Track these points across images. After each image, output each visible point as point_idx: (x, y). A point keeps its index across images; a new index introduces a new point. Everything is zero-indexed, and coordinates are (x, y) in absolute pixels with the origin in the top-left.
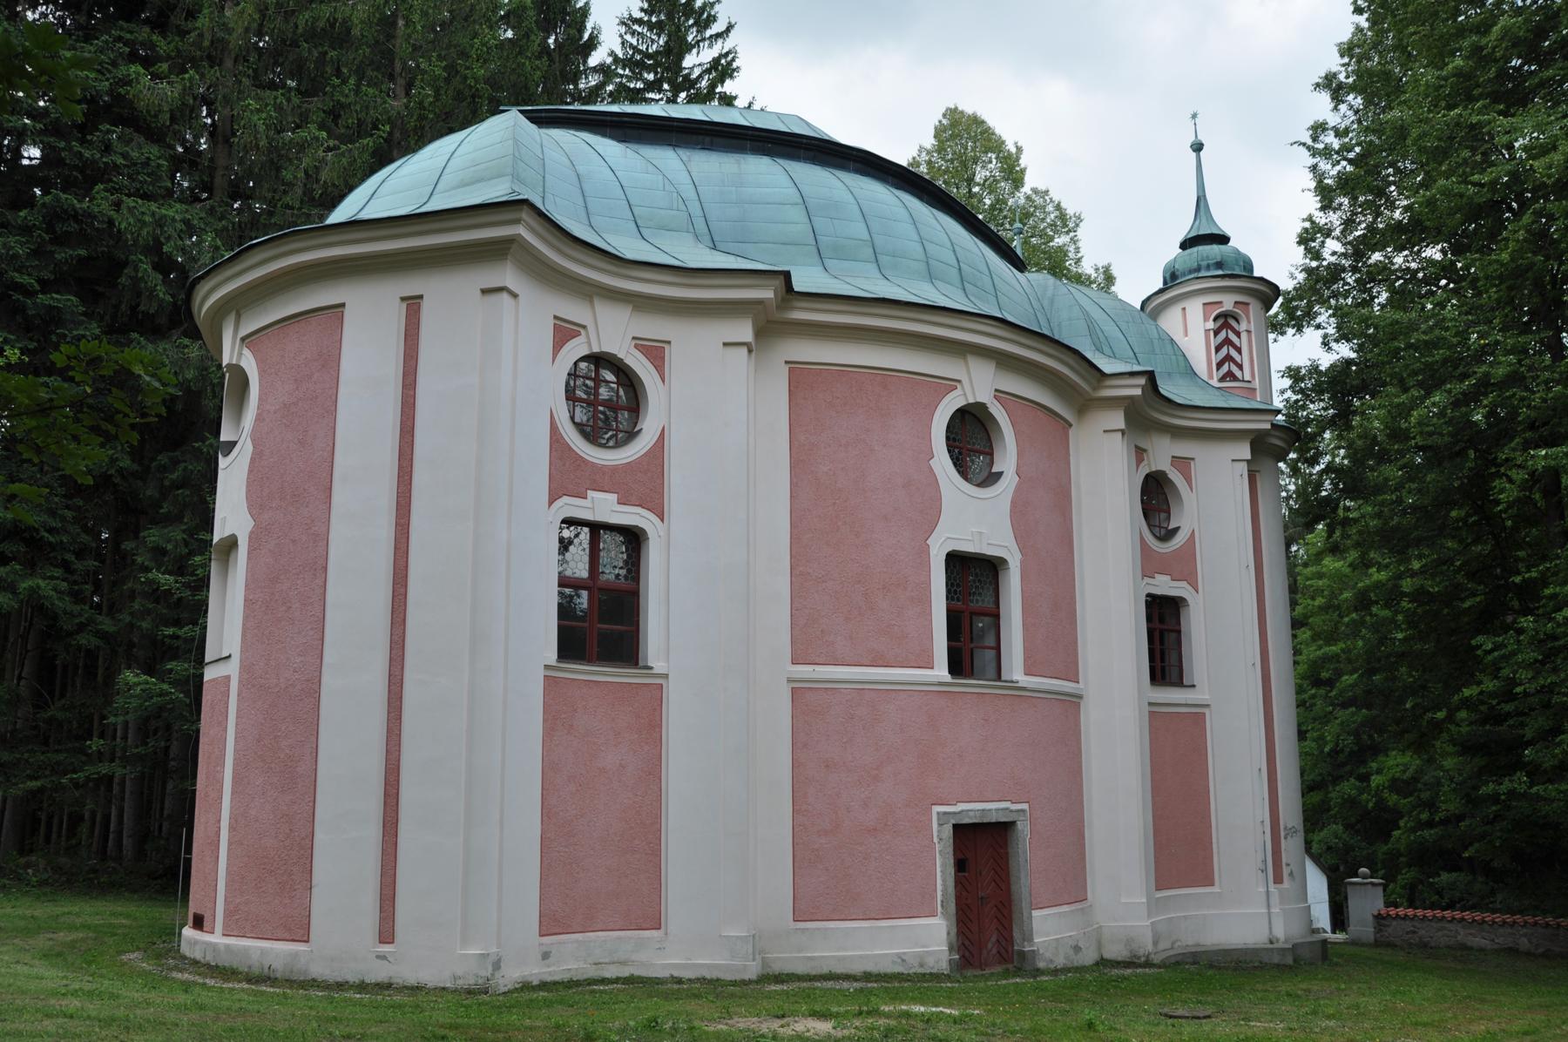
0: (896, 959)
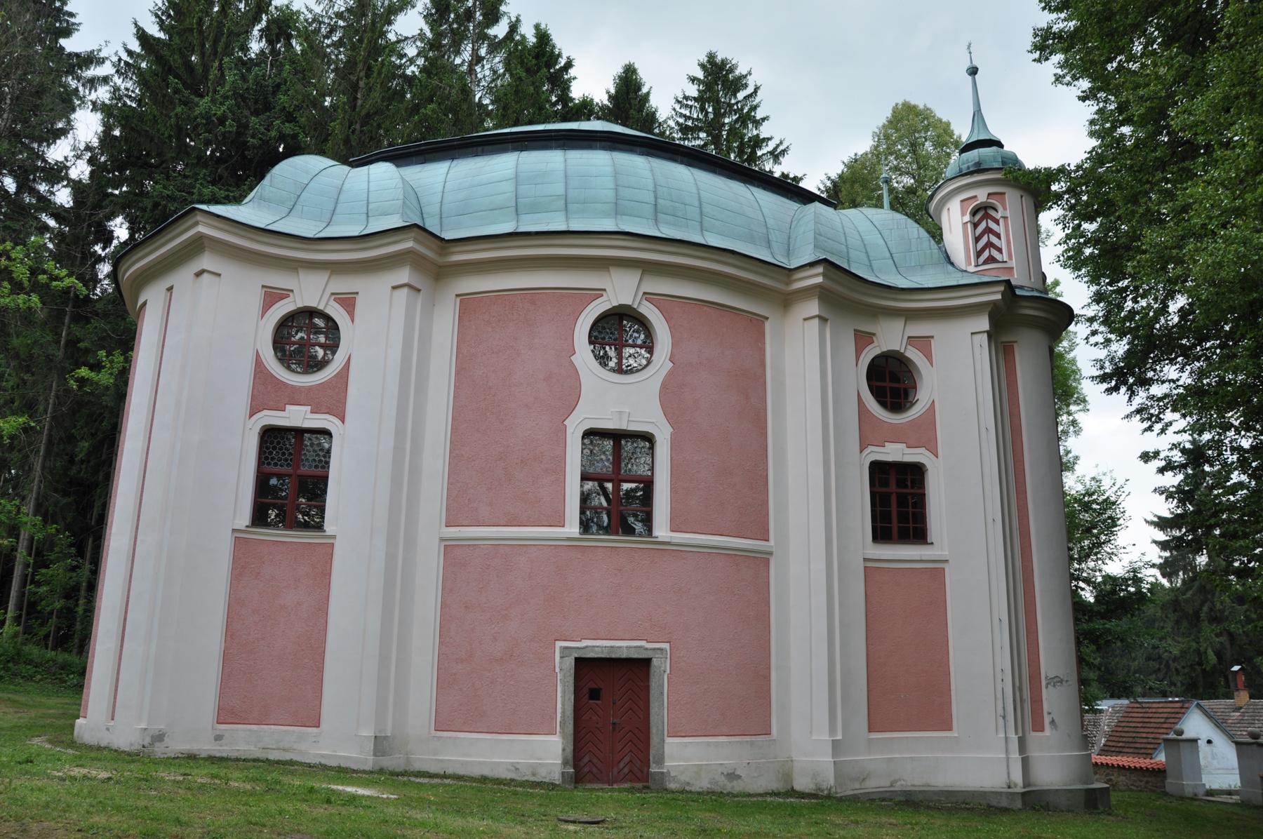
0: (510, 767)
